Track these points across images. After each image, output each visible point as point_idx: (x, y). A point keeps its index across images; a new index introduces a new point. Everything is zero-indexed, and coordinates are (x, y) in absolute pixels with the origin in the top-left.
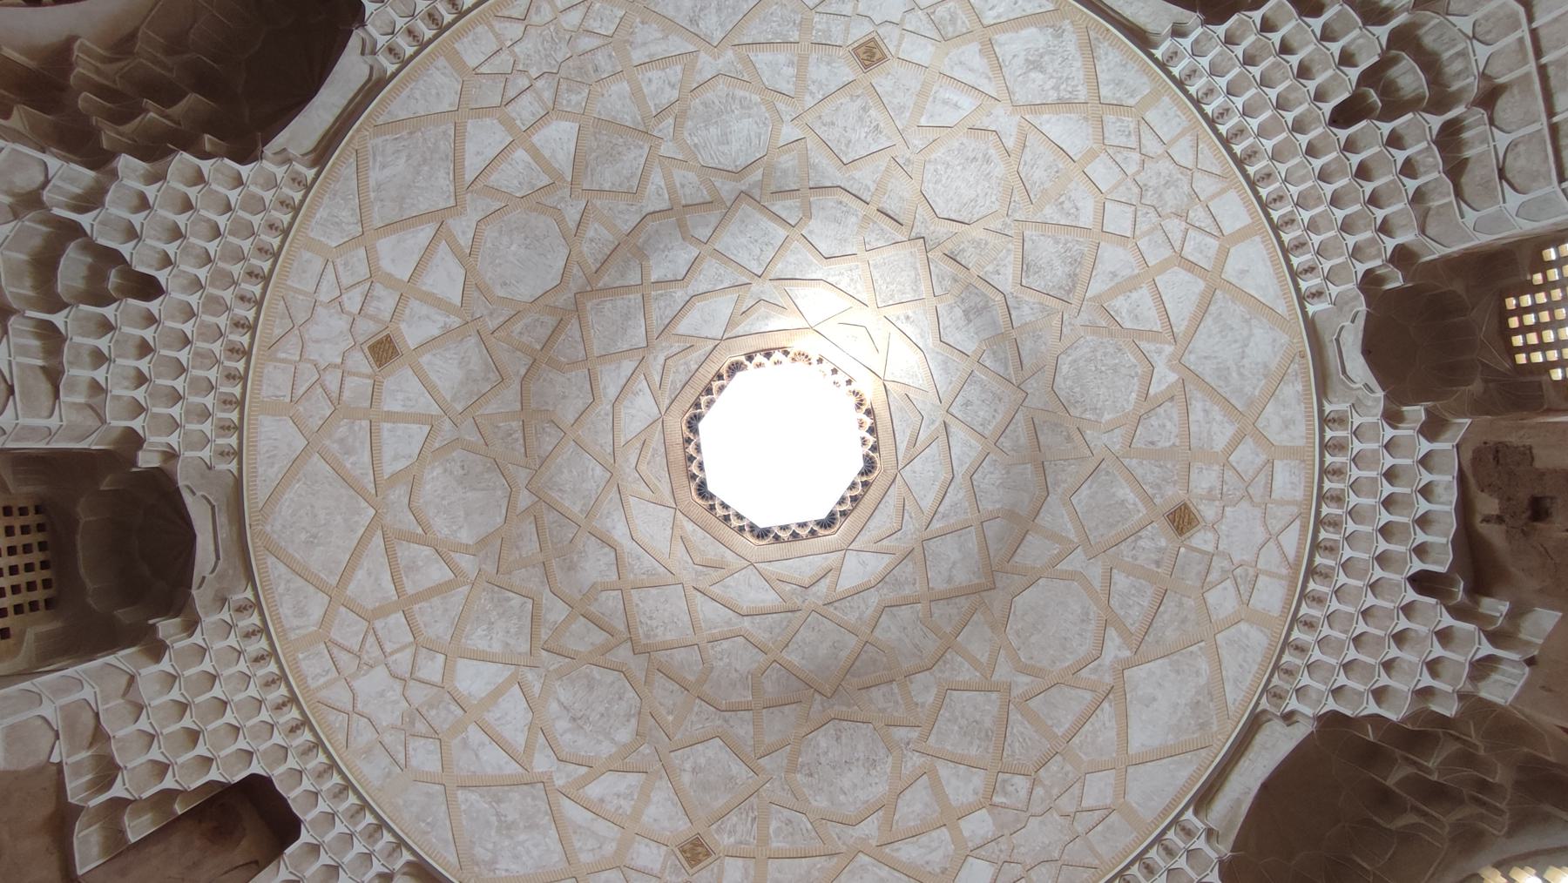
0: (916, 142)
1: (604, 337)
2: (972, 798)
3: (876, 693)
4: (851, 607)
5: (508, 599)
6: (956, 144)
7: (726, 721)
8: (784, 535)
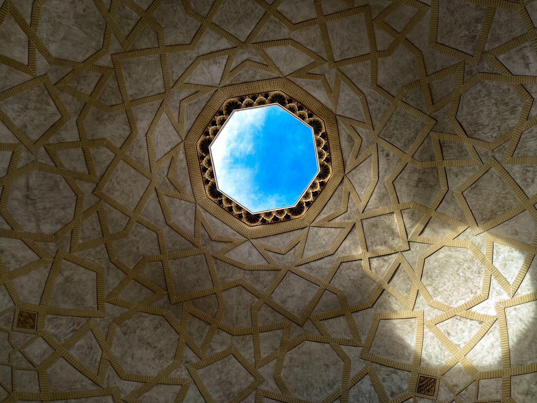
0: (486, 65)
1: (226, 15)
3: (196, 323)
4: (224, 269)
5: (48, 104)
6: (506, 87)
7: (108, 268)
8: (225, 205)
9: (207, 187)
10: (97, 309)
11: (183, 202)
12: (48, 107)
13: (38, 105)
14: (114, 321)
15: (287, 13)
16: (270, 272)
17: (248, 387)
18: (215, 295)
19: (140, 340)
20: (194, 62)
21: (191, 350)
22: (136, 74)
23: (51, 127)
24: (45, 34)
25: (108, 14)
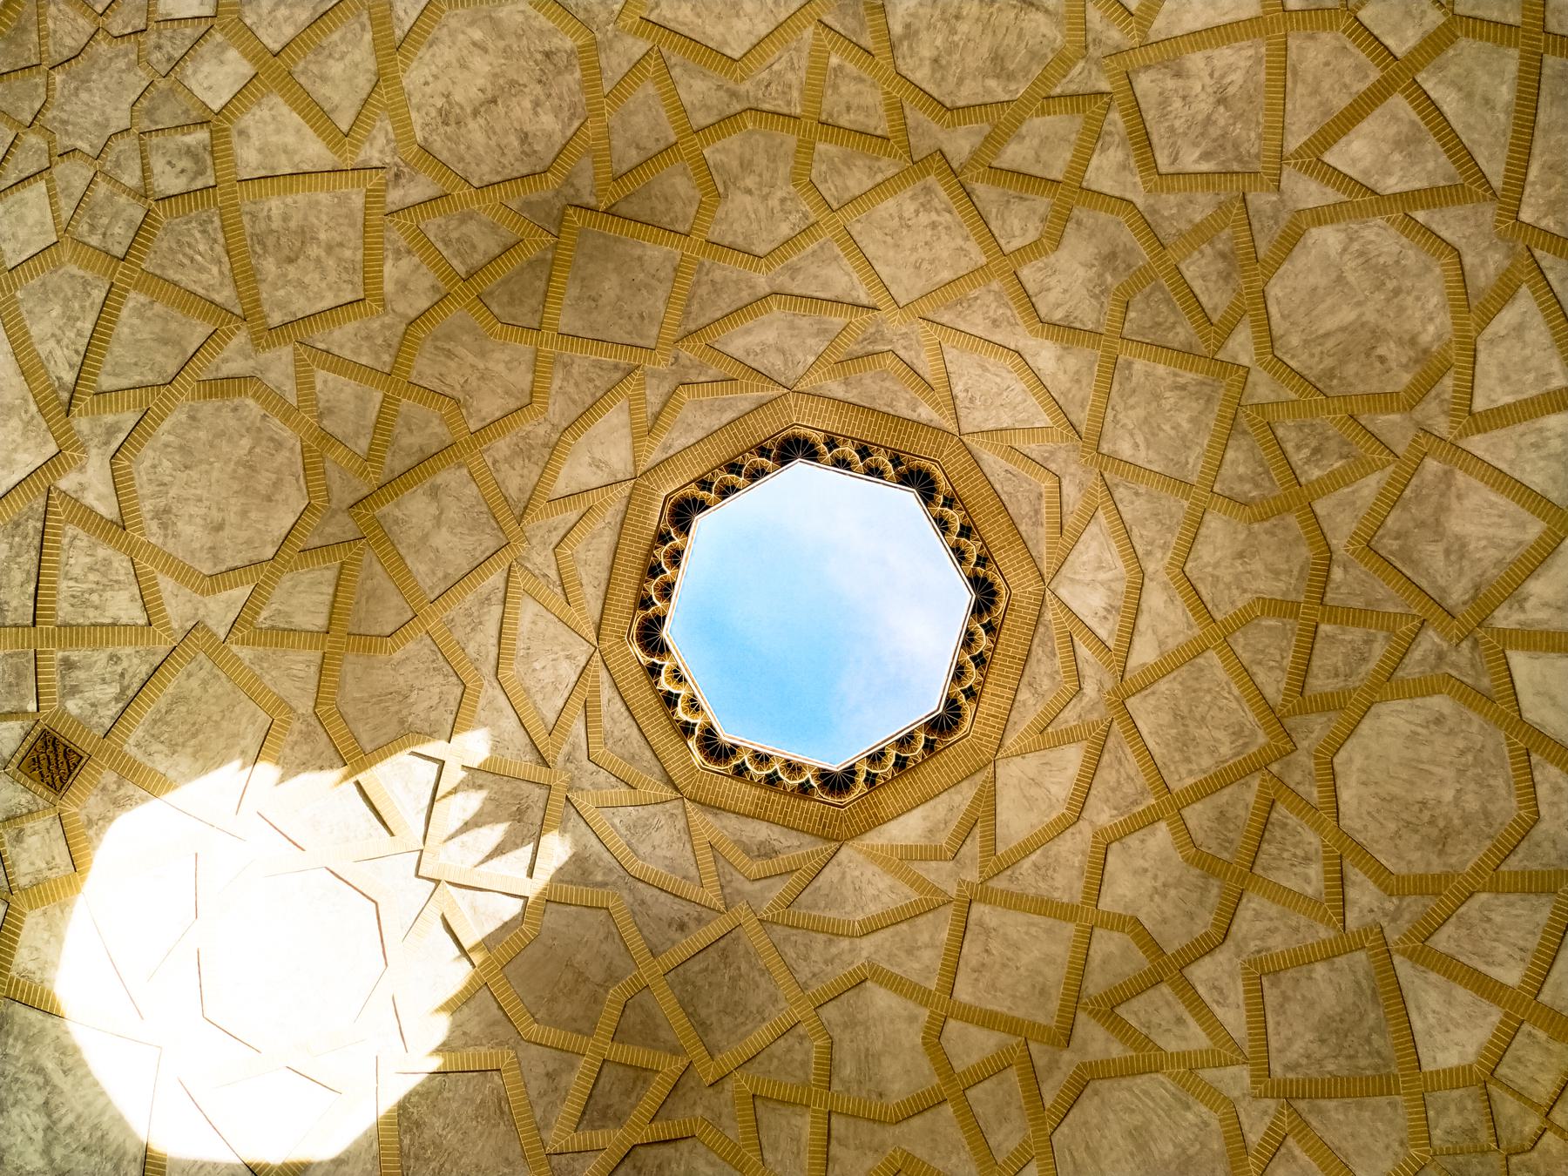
1: (1209, 691)
2: (247, 121)
3: (487, 245)
4: (591, 380)
5: (1206, 156)
7: (733, 94)
9: (818, 438)
10: (644, 15)
11: (811, 359)
12: (1197, 154)
13: (1214, 132)
14: (595, 43)
15: (1143, 841)
16: (529, 493)
17: (258, 300)
18: (536, 325)
19: (513, 83)
20: (1134, 558)
21: (425, 198)
22: (1176, 404)
23: (1147, 133)
24: (1372, 237)
25: (1346, 411)
